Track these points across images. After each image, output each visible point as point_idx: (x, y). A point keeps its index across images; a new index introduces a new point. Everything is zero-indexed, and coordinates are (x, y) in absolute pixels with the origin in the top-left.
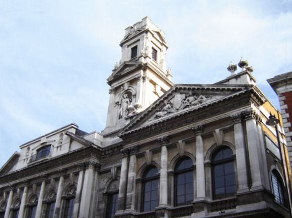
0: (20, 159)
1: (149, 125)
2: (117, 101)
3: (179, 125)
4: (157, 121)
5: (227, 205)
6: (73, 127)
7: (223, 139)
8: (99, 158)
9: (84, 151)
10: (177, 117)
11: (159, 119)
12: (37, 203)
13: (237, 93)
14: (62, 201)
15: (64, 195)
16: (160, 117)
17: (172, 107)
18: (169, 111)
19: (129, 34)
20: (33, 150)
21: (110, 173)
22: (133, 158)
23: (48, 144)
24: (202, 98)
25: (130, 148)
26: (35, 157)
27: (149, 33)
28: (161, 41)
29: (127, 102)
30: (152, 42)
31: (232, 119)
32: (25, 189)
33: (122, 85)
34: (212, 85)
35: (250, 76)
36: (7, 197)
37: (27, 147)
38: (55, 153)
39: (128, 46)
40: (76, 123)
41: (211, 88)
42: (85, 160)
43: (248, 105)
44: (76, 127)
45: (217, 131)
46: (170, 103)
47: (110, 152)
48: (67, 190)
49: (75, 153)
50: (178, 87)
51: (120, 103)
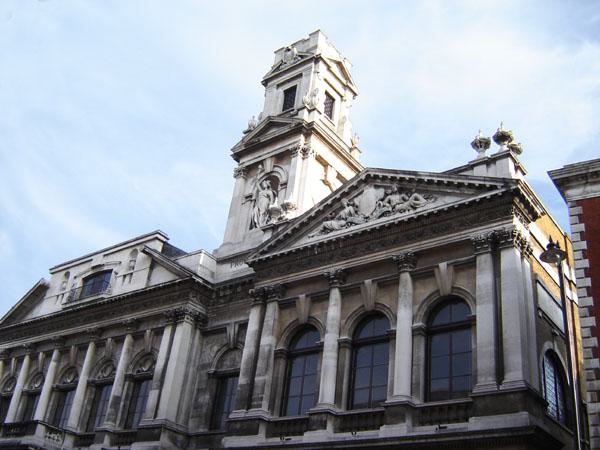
0: (49, 294)
1: (309, 245)
2: (247, 193)
3: (369, 250)
4: (324, 238)
5: (453, 415)
6: (157, 238)
7: (453, 283)
8: (205, 303)
9: (177, 287)
10: (364, 233)
11: (331, 234)
12: (77, 382)
13: (488, 195)
14: (127, 383)
15: (130, 372)
16: (332, 230)
17: (356, 212)
18: (350, 219)
19: (282, 63)
20: (75, 277)
21: (224, 335)
22: (272, 309)
23: (106, 268)
24: (416, 199)
25: (269, 287)
26: (78, 292)
27: (321, 63)
28: (344, 81)
29: (268, 196)
30: (325, 80)
31: (475, 245)
32: (55, 354)
33: (261, 162)
34: (438, 175)
35: (515, 162)
36: (18, 368)
37: (64, 272)
38: (118, 288)
39: (279, 86)
40: (164, 231)
41: (436, 179)
42: (177, 306)
43: (507, 219)
44: (165, 240)
45: (443, 266)
46: (353, 205)
47: (228, 292)
48: (137, 362)
49: (158, 289)
50: (372, 174)
51: (253, 198)
